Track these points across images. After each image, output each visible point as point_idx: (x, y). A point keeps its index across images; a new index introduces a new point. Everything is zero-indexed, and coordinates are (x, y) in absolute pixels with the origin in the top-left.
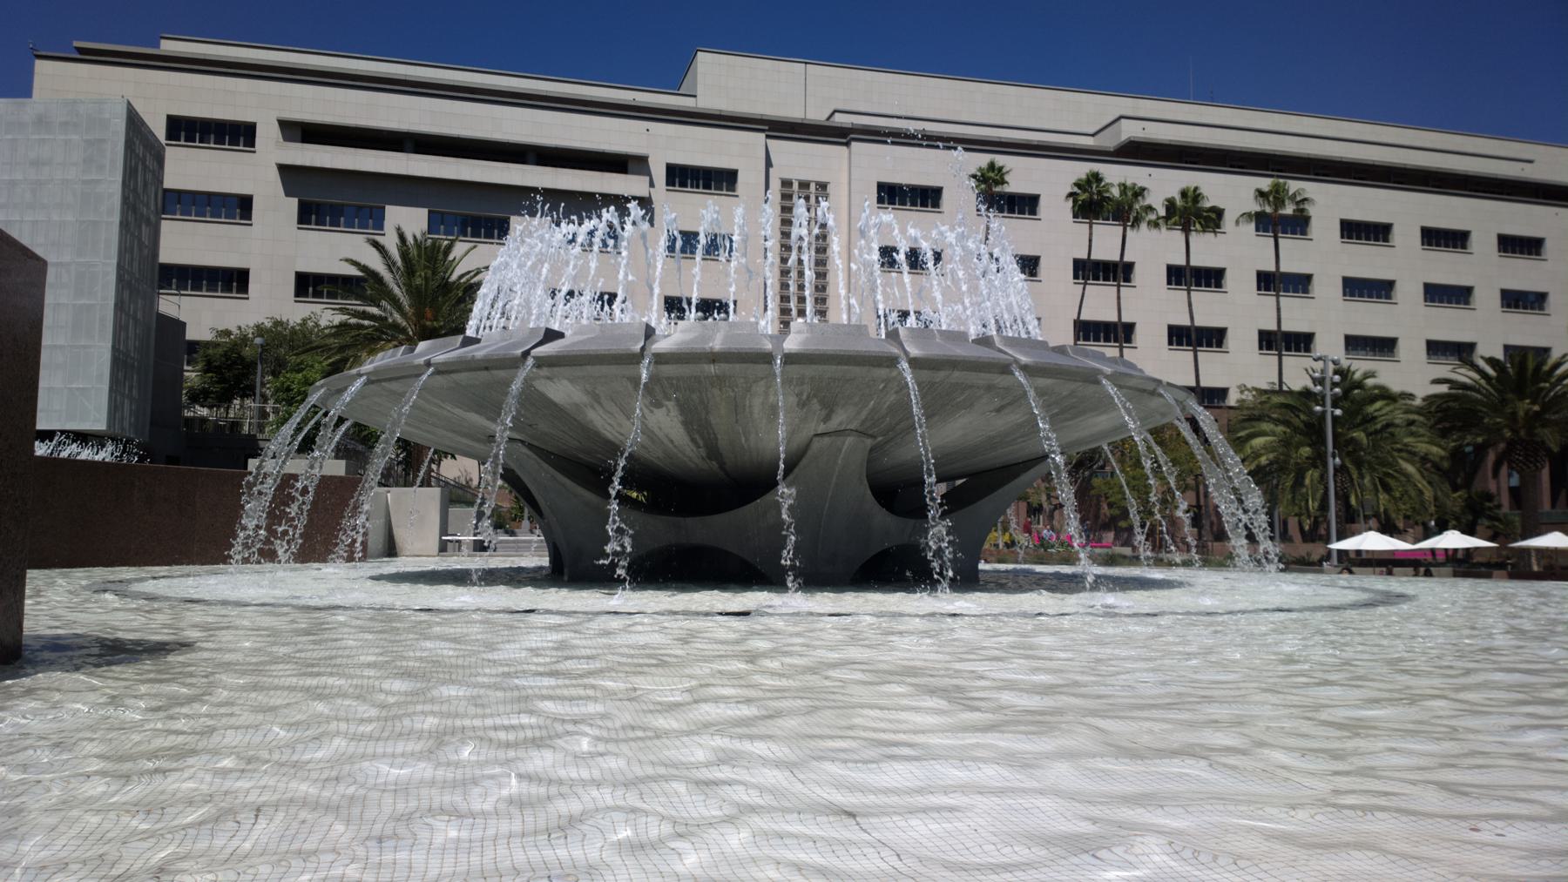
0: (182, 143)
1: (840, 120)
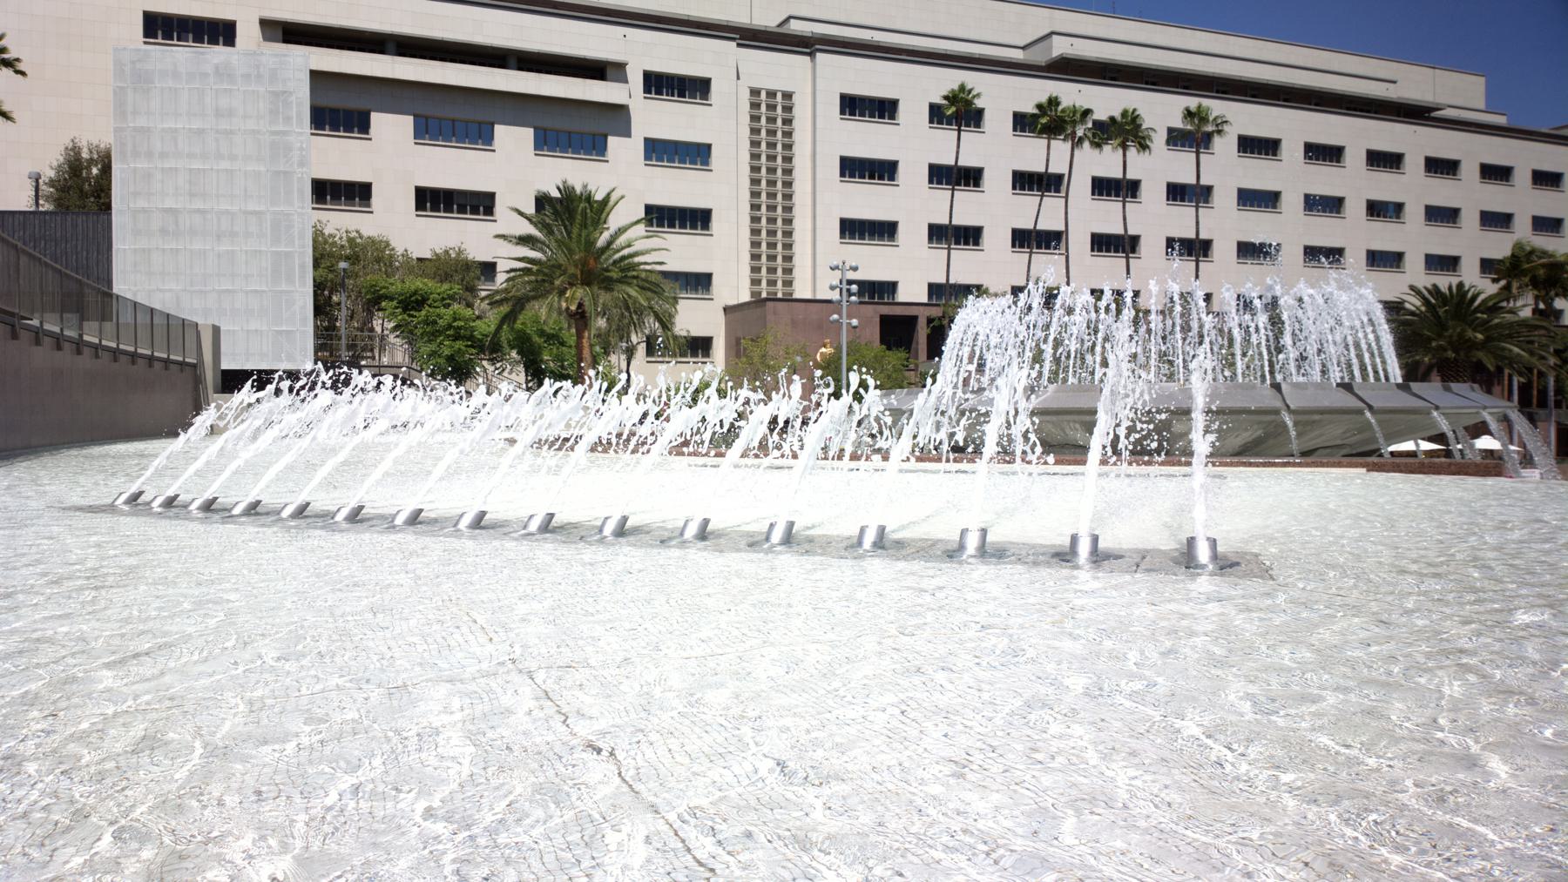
0: (160, 41)
1: (796, 27)
